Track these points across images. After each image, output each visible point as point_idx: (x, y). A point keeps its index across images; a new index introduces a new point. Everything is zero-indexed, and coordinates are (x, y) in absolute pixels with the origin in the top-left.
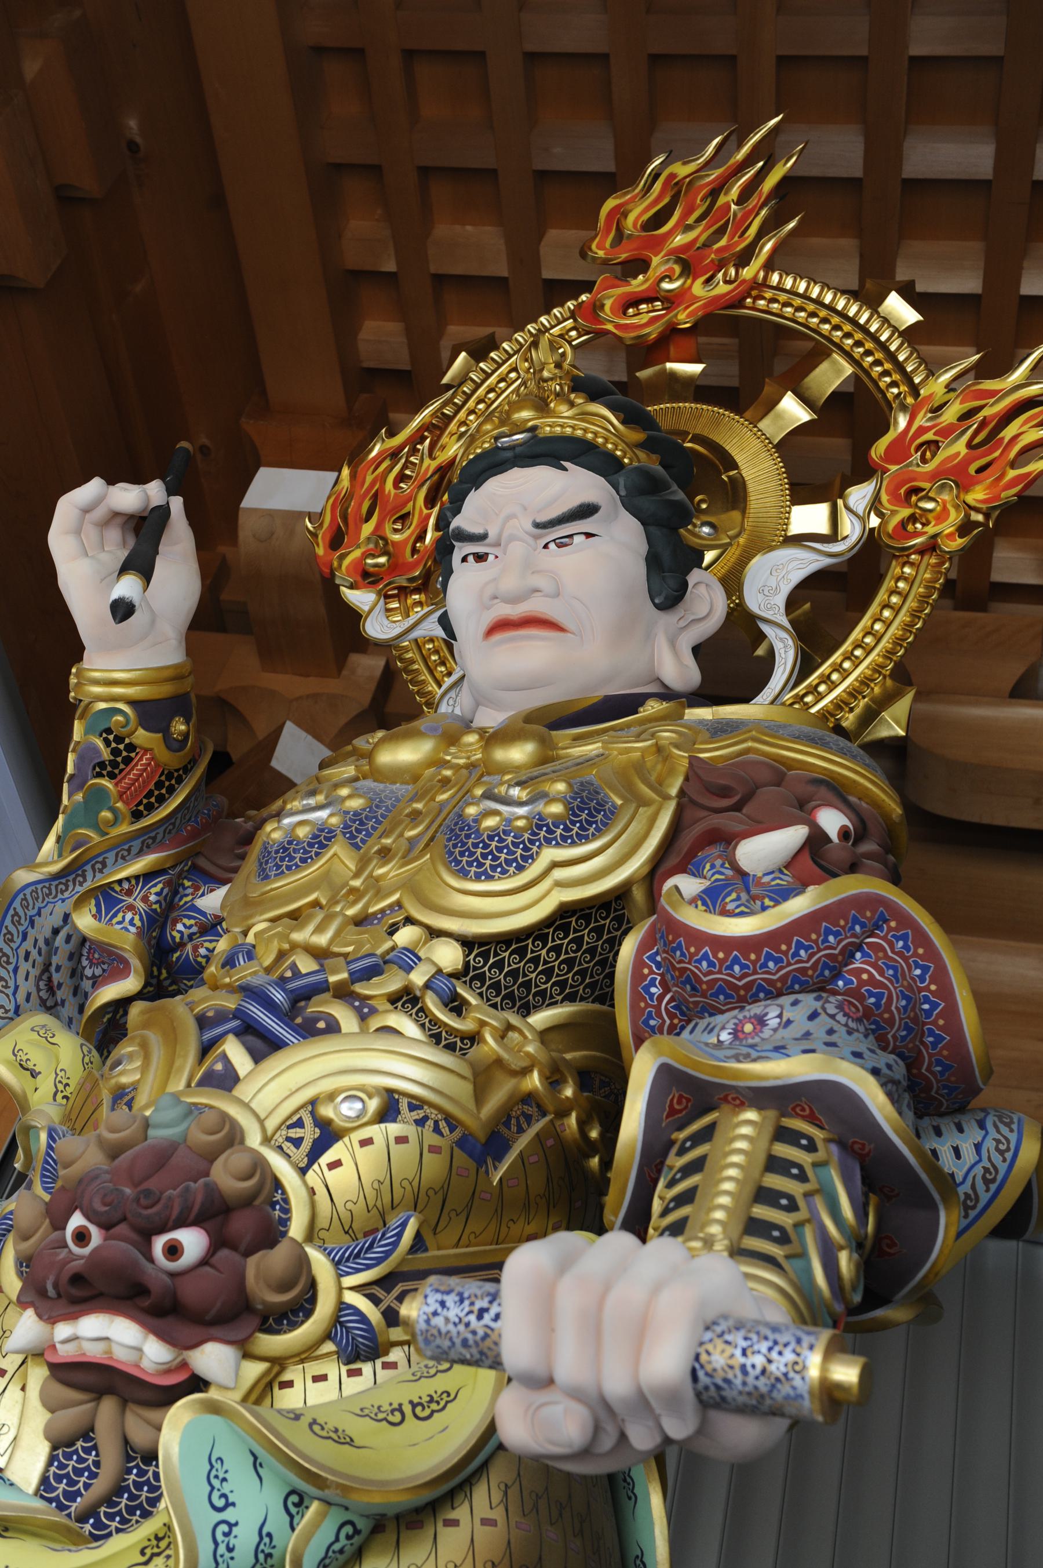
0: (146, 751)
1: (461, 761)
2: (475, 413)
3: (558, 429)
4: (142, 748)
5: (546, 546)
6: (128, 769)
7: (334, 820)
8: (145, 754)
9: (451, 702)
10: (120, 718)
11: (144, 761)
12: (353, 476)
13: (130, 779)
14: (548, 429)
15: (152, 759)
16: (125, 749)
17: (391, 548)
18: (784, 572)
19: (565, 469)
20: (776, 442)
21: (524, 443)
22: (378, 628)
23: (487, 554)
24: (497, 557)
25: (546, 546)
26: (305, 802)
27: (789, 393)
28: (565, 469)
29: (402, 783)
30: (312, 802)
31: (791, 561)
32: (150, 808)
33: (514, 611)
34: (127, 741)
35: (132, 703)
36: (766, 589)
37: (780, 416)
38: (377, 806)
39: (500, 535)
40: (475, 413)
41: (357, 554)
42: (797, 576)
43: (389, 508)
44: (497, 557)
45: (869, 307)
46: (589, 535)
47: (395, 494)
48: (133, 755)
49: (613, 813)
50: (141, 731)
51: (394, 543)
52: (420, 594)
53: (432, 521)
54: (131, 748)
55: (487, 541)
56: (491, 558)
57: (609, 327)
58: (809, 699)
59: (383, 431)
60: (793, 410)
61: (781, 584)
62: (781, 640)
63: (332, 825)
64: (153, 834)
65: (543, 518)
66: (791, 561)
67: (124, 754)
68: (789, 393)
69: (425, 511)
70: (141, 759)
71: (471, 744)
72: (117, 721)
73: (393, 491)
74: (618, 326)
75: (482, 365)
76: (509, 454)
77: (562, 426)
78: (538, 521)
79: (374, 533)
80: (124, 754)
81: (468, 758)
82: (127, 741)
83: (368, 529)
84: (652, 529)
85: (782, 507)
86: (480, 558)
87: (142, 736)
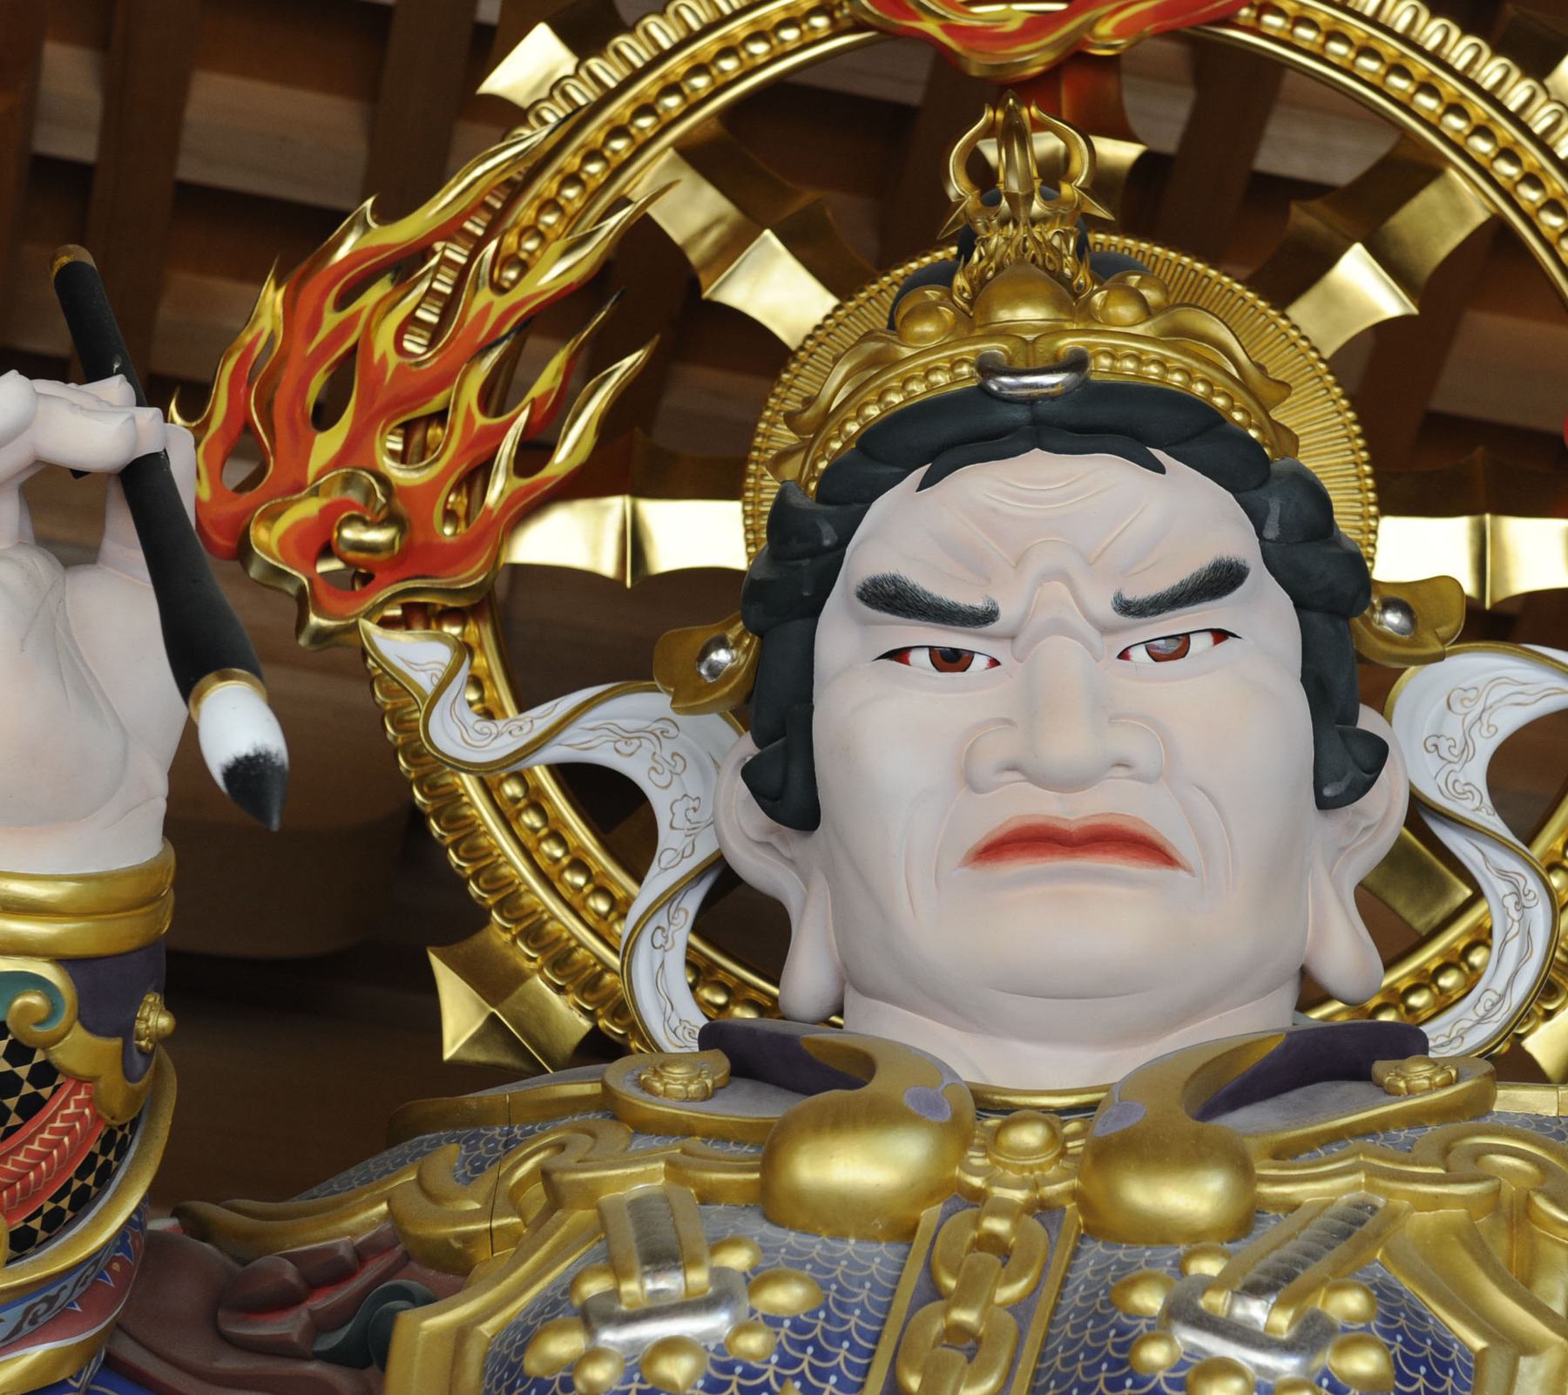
0: (80, 1081)
1: (1019, 1196)
2: (582, 183)
3: (1129, 364)
4: (71, 1075)
5: (1124, 655)
6: (31, 1128)
7: (753, 1343)
8: (75, 1091)
9: (659, 940)
10: (35, 1000)
11: (72, 1109)
12: (290, 305)
13: (29, 1153)
14: (1105, 362)
15: (89, 1102)
16: (31, 1079)
17: (399, 505)
18: (1479, 708)
19: (1160, 469)
20: (1327, 355)
21: (1065, 395)
22: (455, 732)
23: (972, 654)
24: (994, 663)
25: (1124, 655)
26: (650, 1285)
27: (1358, 248)
28: (1160, 469)
29: (863, 1238)
30: (669, 1283)
31: (1496, 681)
32: (55, 1223)
33: (1070, 811)
34: (39, 1057)
35: (65, 962)
36: (1444, 745)
37: (1335, 298)
38: (841, 1306)
39: (1025, 618)
40: (582, 183)
41: (307, 509)
42: (1509, 720)
43: (382, 398)
44: (994, 663)
45: (1527, 72)
46: (1220, 635)
47: (399, 367)
48: (45, 1092)
49: (1467, 1370)
50: (79, 1034)
51: (406, 492)
52: (464, 623)
53: (508, 447)
54: (46, 1074)
55: (991, 628)
56: (979, 663)
57: (930, 27)
58: (1449, 980)
59: (369, 203)
60: (1363, 289)
61: (1475, 733)
62: (1503, 874)
63: (752, 1356)
64: (53, 1292)
65: (1139, 592)
66: (1496, 681)
67: (28, 1089)
68: (1358, 248)
69: (481, 420)
70: (65, 1105)
71: (1030, 1152)
72: (27, 1008)
73: (393, 360)
74: (950, 29)
75: (593, 63)
76: (1020, 414)
77: (1136, 358)
78: (1128, 596)
79: (339, 460)
80: (28, 1089)
81: (1036, 1186)
82: (39, 1057)
83: (328, 444)
84: (1315, 617)
85: (1362, 516)
86: (950, 660)
87: (77, 1049)
